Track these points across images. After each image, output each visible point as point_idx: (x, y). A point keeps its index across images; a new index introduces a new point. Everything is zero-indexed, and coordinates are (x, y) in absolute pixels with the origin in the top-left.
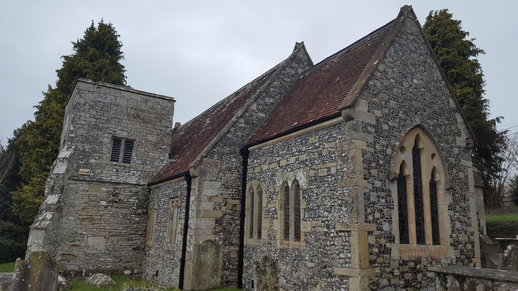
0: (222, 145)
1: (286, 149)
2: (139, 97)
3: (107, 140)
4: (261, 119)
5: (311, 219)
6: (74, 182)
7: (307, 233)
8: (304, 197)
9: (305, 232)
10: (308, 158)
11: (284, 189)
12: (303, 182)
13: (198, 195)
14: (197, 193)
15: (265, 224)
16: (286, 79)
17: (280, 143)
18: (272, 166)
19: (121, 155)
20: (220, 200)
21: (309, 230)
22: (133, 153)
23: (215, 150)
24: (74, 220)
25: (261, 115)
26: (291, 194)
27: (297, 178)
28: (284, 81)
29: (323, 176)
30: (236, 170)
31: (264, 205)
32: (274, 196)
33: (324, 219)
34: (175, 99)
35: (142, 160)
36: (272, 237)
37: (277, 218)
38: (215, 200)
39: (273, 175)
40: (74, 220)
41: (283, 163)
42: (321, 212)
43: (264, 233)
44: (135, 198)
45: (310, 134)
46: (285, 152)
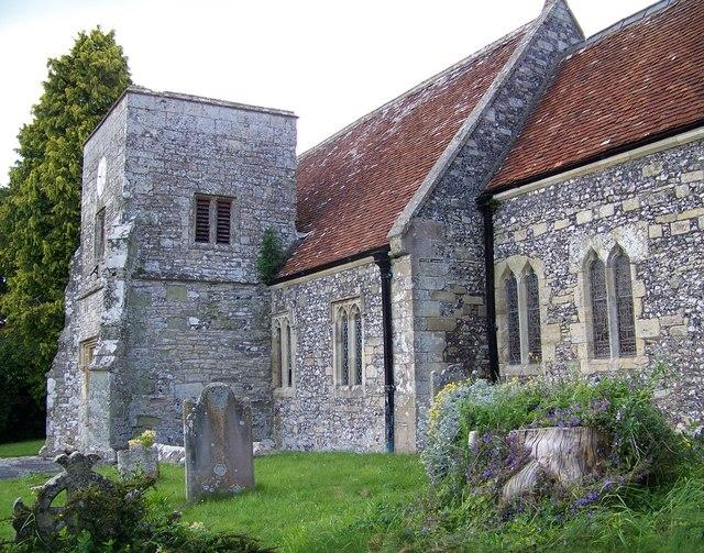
0: (443, 191)
1: (588, 190)
2: (232, 115)
3: (186, 203)
4: (503, 140)
5: (659, 314)
6: (141, 284)
7: (650, 339)
8: (638, 278)
9: (645, 339)
10: (643, 204)
11: (588, 265)
12: (636, 249)
13: (413, 289)
14: (410, 286)
15: (549, 333)
16: (539, 62)
17: (572, 181)
18: (558, 225)
19: (213, 230)
20: (449, 297)
21: (656, 334)
22: (232, 223)
23: (434, 202)
24: (149, 354)
25: (505, 131)
26: (607, 275)
27: (621, 243)
28: (536, 65)
29: (682, 235)
30: (471, 241)
31: (543, 300)
32: (568, 282)
33: (688, 311)
34: (296, 114)
35: (250, 236)
36: (566, 355)
37: (578, 321)
38: (442, 296)
39: (561, 242)
40: (149, 354)
41: (584, 217)
42: (681, 298)
43: (548, 353)
44: (246, 309)
45: (645, 160)
46: (587, 196)
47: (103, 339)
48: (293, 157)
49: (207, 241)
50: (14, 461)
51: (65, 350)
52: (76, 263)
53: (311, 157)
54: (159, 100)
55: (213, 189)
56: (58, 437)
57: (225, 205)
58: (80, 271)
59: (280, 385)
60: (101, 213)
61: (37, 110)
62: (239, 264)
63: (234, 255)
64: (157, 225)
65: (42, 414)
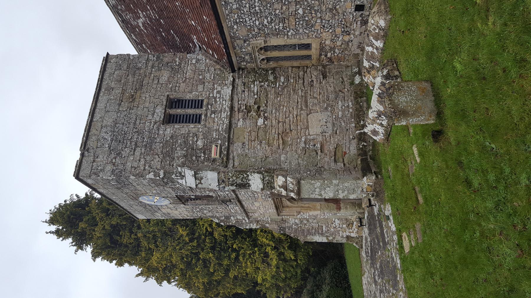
2: (103, 98)
3: (169, 130)
6: (231, 161)
24: (286, 154)
40: (286, 154)
44: (252, 86)
47: (274, 188)
48: (139, 57)
49: (200, 116)
50: (366, 267)
51: (285, 228)
52: (222, 221)
53: (136, 44)
54: (86, 153)
55: (160, 111)
56: (348, 234)
57: (173, 103)
58: (228, 218)
59: (309, 57)
60: (182, 200)
61: (120, 264)
62: (219, 92)
63: (211, 95)
64: (187, 151)
65: (329, 245)
